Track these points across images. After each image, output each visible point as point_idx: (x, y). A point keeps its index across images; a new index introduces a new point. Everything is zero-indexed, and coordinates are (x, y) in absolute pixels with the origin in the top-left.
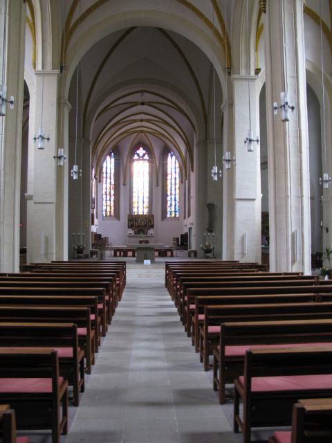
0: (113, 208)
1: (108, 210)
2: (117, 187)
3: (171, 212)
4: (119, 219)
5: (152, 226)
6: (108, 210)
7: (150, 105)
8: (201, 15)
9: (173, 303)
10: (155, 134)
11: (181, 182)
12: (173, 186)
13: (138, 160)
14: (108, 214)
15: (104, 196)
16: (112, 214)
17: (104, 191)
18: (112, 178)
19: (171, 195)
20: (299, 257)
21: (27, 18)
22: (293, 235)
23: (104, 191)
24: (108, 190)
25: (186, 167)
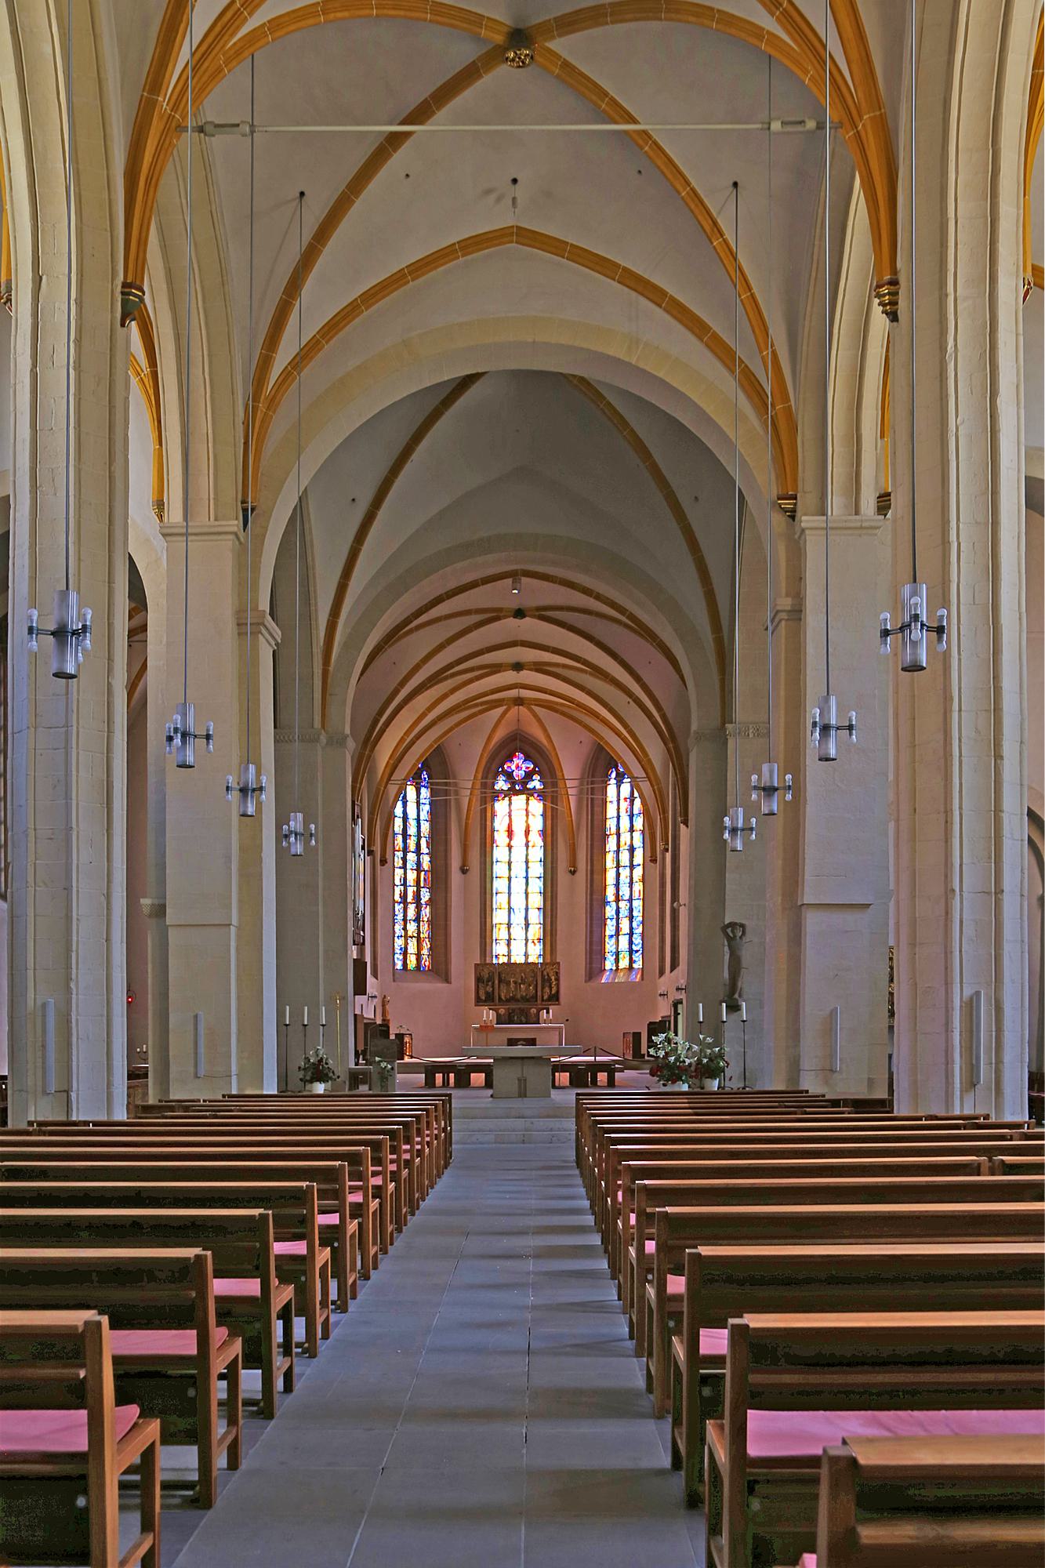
0: (426, 945)
1: (412, 948)
3: (617, 954)
5: (555, 998)
6: (412, 948)
11: (651, 858)
12: (625, 873)
13: (512, 792)
14: (412, 962)
15: (398, 908)
16: (426, 962)
17: (398, 890)
18: (424, 849)
19: (618, 899)
20: (985, 1072)
21: (130, 357)
22: (971, 1007)
23: (398, 890)
24: (411, 891)
25: (664, 811)
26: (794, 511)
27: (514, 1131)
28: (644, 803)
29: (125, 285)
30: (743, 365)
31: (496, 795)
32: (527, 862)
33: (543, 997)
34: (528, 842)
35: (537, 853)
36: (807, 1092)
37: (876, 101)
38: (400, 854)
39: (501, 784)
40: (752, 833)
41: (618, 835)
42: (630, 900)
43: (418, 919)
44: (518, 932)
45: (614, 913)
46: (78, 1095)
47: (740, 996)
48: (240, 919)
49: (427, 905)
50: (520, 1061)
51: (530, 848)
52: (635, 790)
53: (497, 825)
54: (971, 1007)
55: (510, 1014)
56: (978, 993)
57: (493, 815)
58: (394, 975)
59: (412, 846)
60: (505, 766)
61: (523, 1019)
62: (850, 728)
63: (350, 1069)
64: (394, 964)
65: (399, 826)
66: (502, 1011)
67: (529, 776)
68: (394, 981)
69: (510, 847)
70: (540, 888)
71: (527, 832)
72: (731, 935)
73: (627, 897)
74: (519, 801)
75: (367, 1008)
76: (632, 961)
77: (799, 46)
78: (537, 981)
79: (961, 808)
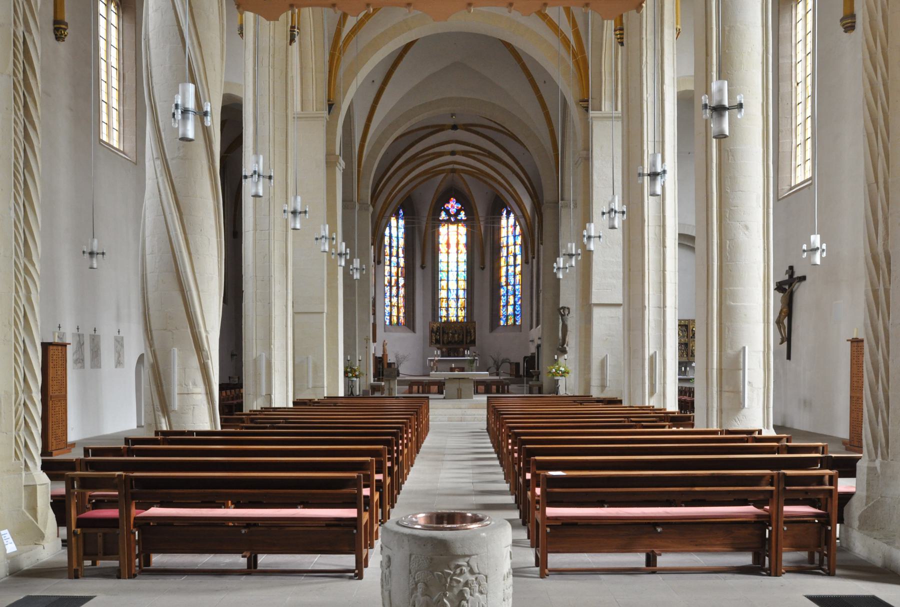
0: (402, 310)
2: (409, 273)
3: (507, 316)
4: (413, 329)
9: (506, 487)
10: (478, 175)
11: (525, 261)
13: (448, 221)
14: (395, 319)
15: (387, 289)
16: (402, 320)
17: (387, 279)
18: (401, 255)
23: (387, 279)
24: (394, 279)
27: (456, 415)
28: (521, 229)
30: (563, 35)
32: (457, 262)
33: (466, 341)
35: (463, 257)
36: (592, 396)
38: (387, 258)
41: (508, 247)
42: (514, 285)
43: (397, 296)
44: (452, 303)
45: (505, 292)
47: (567, 345)
49: (402, 287)
50: (458, 380)
51: (459, 254)
52: (517, 222)
54: (652, 359)
55: (448, 351)
56: (655, 352)
57: (439, 234)
58: (385, 328)
59: (394, 253)
60: (445, 206)
61: (456, 355)
63: (371, 384)
64: (385, 322)
65: (387, 241)
66: (444, 350)
67: (458, 212)
68: (385, 331)
69: (448, 253)
70: (465, 277)
71: (458, 245)
72: (563, 313)
73: (512, 283)
74: (453, 228)
76: (515, 321)
78: (463, 332)
79: (648, 269)
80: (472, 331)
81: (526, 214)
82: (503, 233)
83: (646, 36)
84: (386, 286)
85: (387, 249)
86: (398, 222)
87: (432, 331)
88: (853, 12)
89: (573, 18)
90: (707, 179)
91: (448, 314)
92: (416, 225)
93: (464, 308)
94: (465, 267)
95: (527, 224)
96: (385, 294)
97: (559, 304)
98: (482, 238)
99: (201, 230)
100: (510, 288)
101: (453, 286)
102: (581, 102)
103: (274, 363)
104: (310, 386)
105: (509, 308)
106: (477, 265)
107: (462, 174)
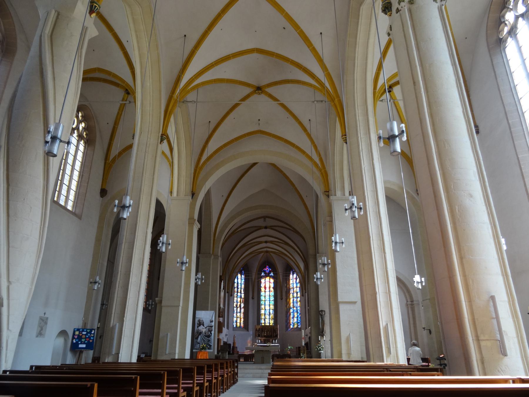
0: (242, 320)
1: (239, 321)
2: (246, 301)
6: (239, 321)
7: (272, 229)
8: (303, 152)
10: (280, 254)
16: (242, 325)
17: (235, 304)
18: (242, 292)
24: (239, 304)
26: (329, 195)
28: (300, 280)
29: (162, 135)
31: (262, 277)
32: (270, 296)
34: (270, 290)
35: (272, 293)
37: (338, 96)
38: (236, 293)
39: (263, 274)
40: (322, 280)
42: (297, 308)
44: (267, 317)
45: (293, 311)
46: (121, 355)
48: (183, 304)
53: (262, 285)
54: (386, 328)
55: (264, 341)
59: (239, 291)
62: (343, 243)
64: (233, 326)
66: (262, 340)
67: (270, 272)
69: (265, 292)
71: (270, 288)
72: (321, 314)
74: (267, 279)
75: (224, 337)
76: (298, 325)
77: (321, 87)
80: (276, 330)
81: (301, 272)
82: (291, 282)
83: (360, 136)
84: (235, 307)
85: (236, 289)
86: (241, 277)
87: (256, 330)
88: (476, 124)
89: (319, 152)
90: (429, 164)
91: (265, 322)
92: (250, 277)
93: (273, 319)
94: (273, 299)
95: (302, 276)
96: (234, 311)
97: (319, 309)
98: (281, 284)
99: (24, 199)
100: (295, 308)
101: (267, 307)
102: (325, 192)
103: (124, 330)
104: (167, 353)
105: (294, 320)
106: (279, 297)
107: (271, 254)
